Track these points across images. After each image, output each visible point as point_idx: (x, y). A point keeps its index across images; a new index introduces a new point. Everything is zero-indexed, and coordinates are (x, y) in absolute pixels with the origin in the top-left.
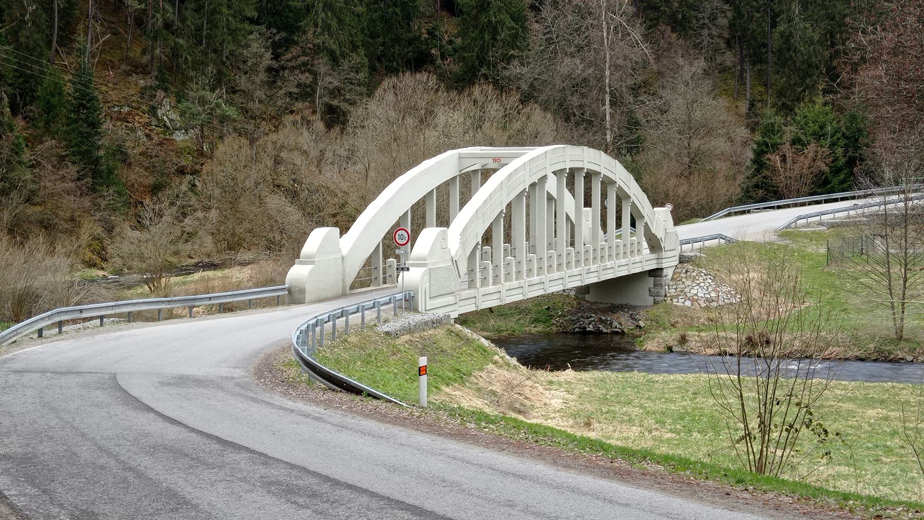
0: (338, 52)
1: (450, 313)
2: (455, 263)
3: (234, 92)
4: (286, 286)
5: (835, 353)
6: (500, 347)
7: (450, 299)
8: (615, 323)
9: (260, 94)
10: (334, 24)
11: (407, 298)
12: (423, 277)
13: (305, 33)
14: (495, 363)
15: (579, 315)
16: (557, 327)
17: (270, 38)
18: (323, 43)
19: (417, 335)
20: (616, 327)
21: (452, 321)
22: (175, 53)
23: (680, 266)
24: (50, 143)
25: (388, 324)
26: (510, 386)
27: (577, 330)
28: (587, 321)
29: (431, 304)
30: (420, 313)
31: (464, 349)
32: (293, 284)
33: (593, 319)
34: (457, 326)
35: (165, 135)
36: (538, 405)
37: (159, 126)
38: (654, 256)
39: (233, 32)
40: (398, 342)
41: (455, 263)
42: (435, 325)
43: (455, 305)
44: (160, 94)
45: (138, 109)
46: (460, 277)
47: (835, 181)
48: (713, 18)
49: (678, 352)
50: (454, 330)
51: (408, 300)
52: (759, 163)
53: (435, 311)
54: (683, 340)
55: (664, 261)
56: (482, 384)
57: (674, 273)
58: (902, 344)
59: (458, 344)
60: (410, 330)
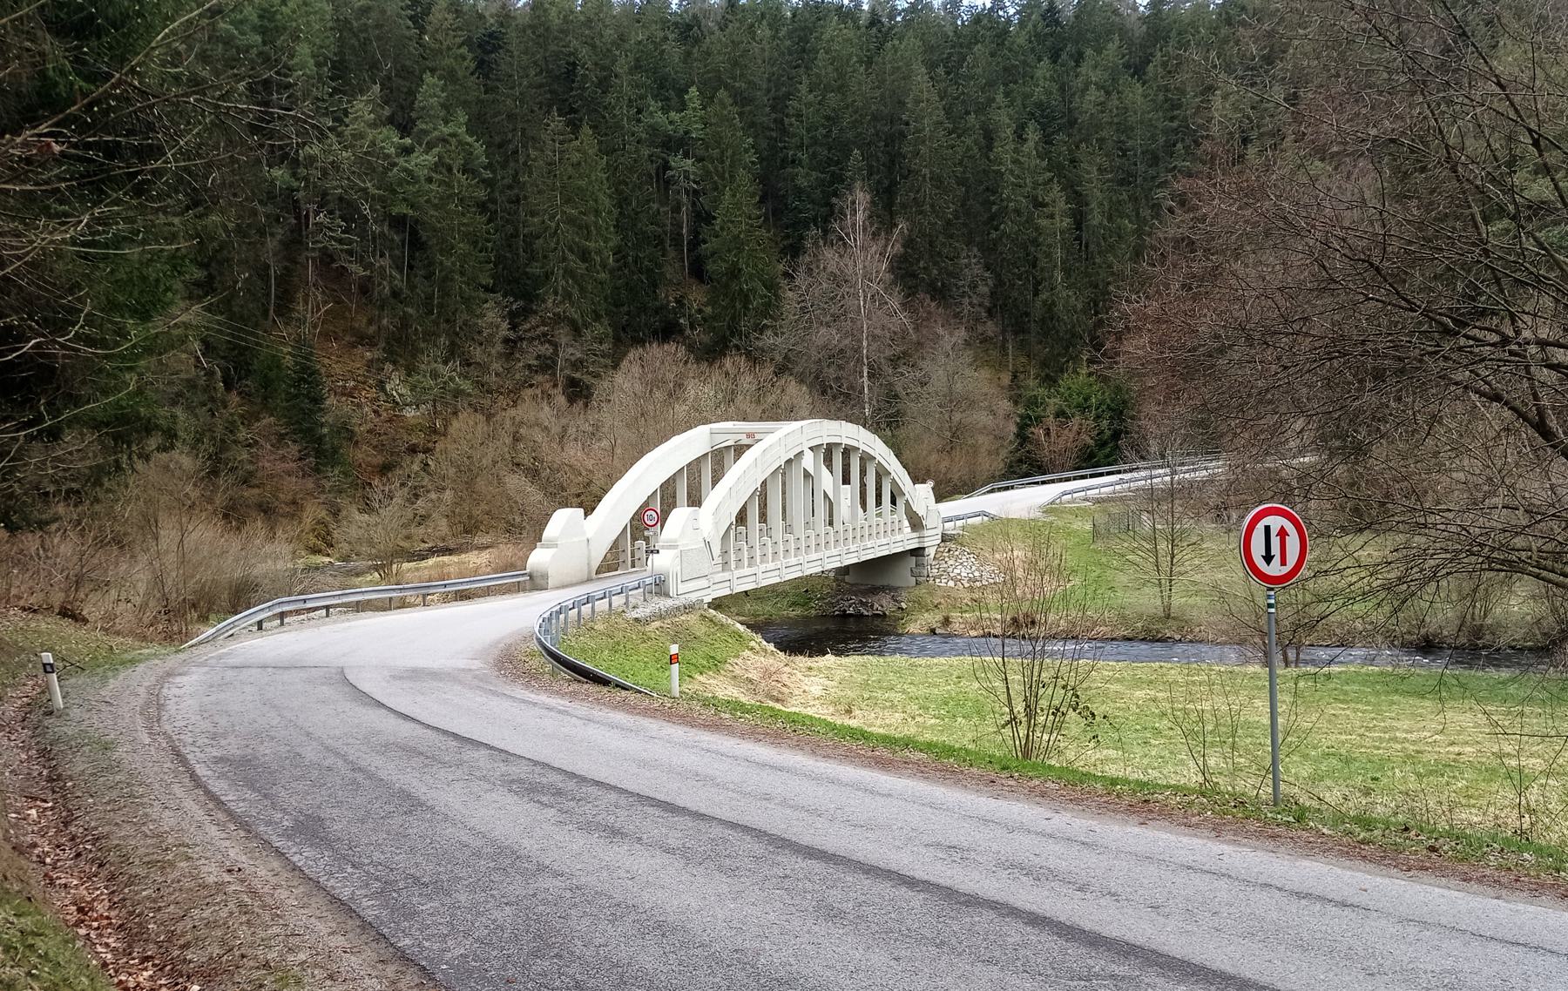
4: (528, 571)
7: (703, 583)
8: (876, 606)
9: (496, 366)
10: (576, 294)
13: (544, 301)
22: (405, 322)
23: (942, 545)
24: (268, 420)
26: (767, 674)
29: (683, 588)
34: (711, 611)
35: (394, 411)
36: (797, 693)
38: (915, 535)
39: (467, 301)
40: (648, 628)
44: (389, 367)
45: (364, 383)
47: (1101, 454)
48: (974, 286)
52: (1022, 437)
53: (687, 596)
54: (946, 621)
55: (926, 539)
56: (738, 671)
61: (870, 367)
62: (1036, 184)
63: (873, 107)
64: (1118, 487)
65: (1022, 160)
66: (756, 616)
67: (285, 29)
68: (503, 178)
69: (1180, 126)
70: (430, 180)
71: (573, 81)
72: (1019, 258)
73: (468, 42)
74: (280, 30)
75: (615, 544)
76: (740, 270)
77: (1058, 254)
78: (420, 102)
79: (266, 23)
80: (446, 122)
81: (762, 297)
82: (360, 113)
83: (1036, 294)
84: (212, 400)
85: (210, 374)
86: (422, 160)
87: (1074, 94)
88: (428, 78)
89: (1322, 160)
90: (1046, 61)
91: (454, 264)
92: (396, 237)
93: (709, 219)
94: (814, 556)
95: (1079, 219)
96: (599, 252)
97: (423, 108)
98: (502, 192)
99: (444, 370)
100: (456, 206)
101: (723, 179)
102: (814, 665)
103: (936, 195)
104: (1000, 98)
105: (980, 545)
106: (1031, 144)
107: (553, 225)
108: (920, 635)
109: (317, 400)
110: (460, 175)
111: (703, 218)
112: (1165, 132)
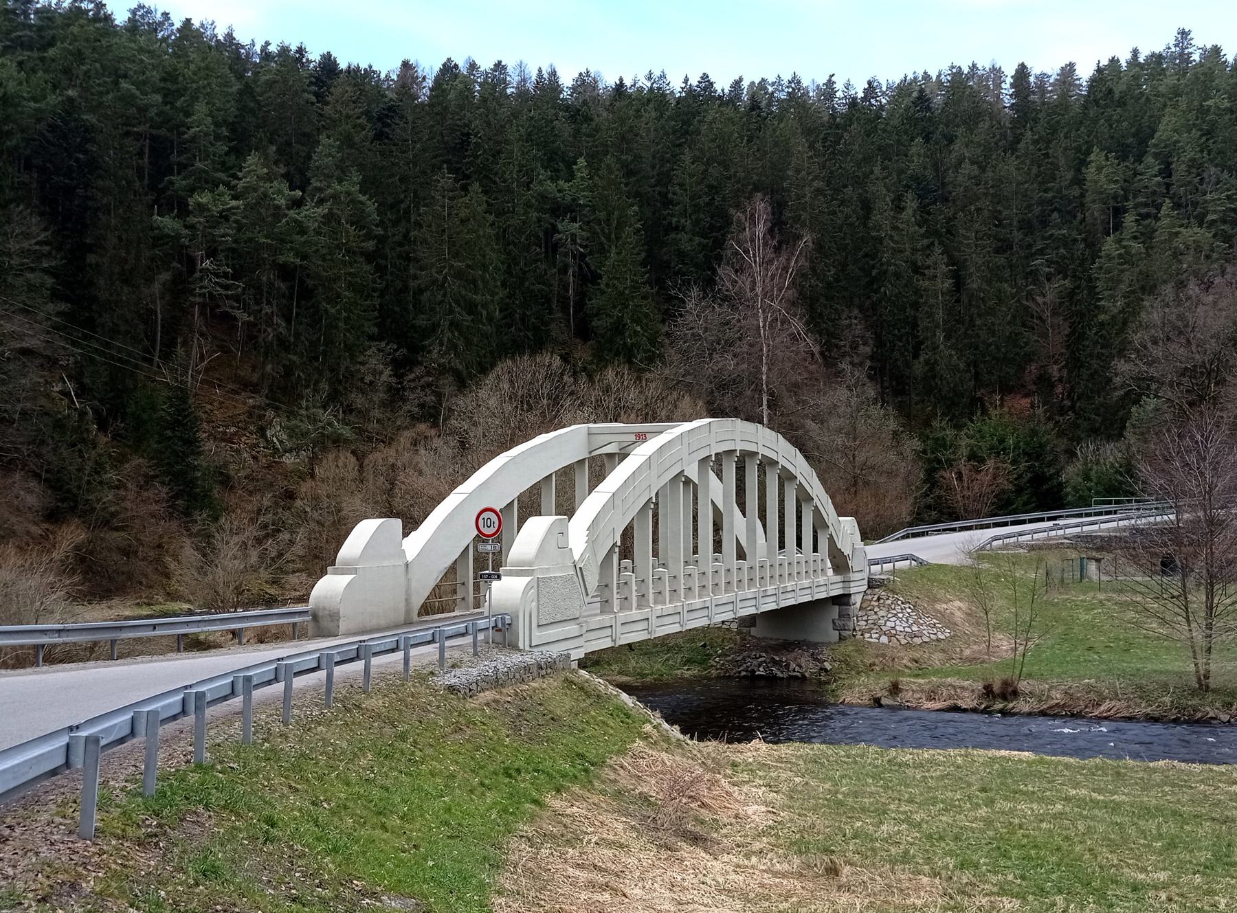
0: (465, 372)
1: (569, 652)
2: (580, 572)
3: (351, 411)
4: (311, 604)
5: (1115, 709)
6: (653, 709)
7: (572, 629)
8: (793, 665)
9: (376, 413)
10: (461, 344)
11: (500, 625)
12: (526, 591)
13: (430, 352)
14: (646, 737)
15: (745, 654)
16: (717, 669)
17: (390, 354)
18: (449, 363)
19: (510, 690)
20: (794, 671)
21: (575, 665)
22: (289, 371)
23: (869, 592)
24: (137, 461)
25: (458, 672)
26: (679, 788)
27: (743, 673)
28: (755, 662)
29: (539, 636)
30: (520, 651)
31: (593, 713)
32: (321, 605)
33: (763, 659)
34: (583, 672)
35: (274, 457)
36: (726, 820)
37: (267, 448)
38: (839, 578)
39: (349, 348)
40: (471, 704)
41: (580, 572)
42: (543, 672)
43: (580, 639)
44: (270, 414)
45: (245, 429)
46: (587, 595)
47: (1020, 501)
48: (855, 347)
49: (888, 707)
50: (576, 680)
51: (500, 630)
52: (931, 480)
53: (544, 649)
54: (895, 689)
55: (852, 584)
56: (625, 782)
57: (863, 601)
58: (1210, 697)
59: (582, 705)
60: (496, 682)
61: (771, 394)
62: (914, 250)
63: (755, 177)
64: (1053, 533)
65: (901, 226)
66: (644, 676)
67: (186, 89)
68: (394, 235)
69: (1054, 197)
70: (319, 233)
71: (467, 150)
72: (900, 320)
73: (367, 113)
74: (180, 93)
75: (452, 569)
76: (624, 325)
77: (940, 315)
78: (316, 161)
79: (169, 85)
80: (340, 181)
81: (646, 351)
82: (253, 167)
83: (916, 356)
84: (83, 441)
85: (82, 414)
86: (312, 213)
87: (948, 169)
88: (323, 139)
89: (1200, 226)
90: (919, 140)
91: (339, 312)
92: (282, 285)
93: (596, 277)
94: (724, 597)
95: (959, 282)
96: (484, 306)
97: (318, 168)
98: (392, 249)
99: (325, 416)
100: (343, 256)
101: (609, 239)
102: (738, 758)
103: (816, 258)
104: (877, 170)
105: (915, 593)
106: (910, 211)
107: (440, 278)
108: (860, 705)
109: (192, 444)
110: (348, 226)
111: (588, 278)
112: (1041, 202)
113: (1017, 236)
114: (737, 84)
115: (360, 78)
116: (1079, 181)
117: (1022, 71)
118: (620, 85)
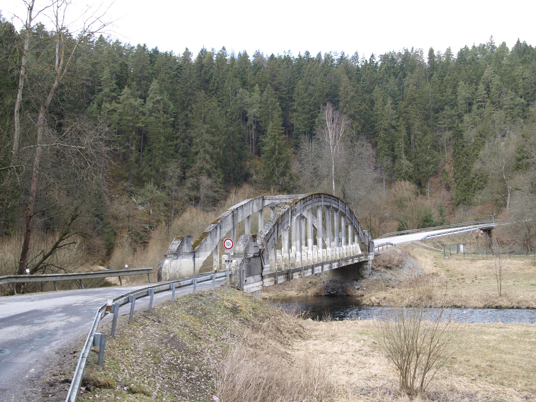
113: (432, 114)
114: (319, 55)
115: (168, 57)
116: (454, 93)
117: (431, 51)
118: (272, 55)
